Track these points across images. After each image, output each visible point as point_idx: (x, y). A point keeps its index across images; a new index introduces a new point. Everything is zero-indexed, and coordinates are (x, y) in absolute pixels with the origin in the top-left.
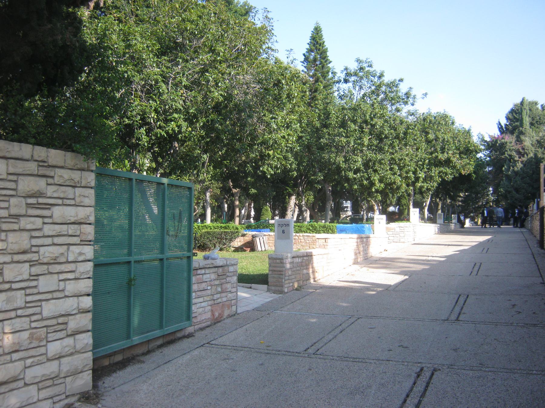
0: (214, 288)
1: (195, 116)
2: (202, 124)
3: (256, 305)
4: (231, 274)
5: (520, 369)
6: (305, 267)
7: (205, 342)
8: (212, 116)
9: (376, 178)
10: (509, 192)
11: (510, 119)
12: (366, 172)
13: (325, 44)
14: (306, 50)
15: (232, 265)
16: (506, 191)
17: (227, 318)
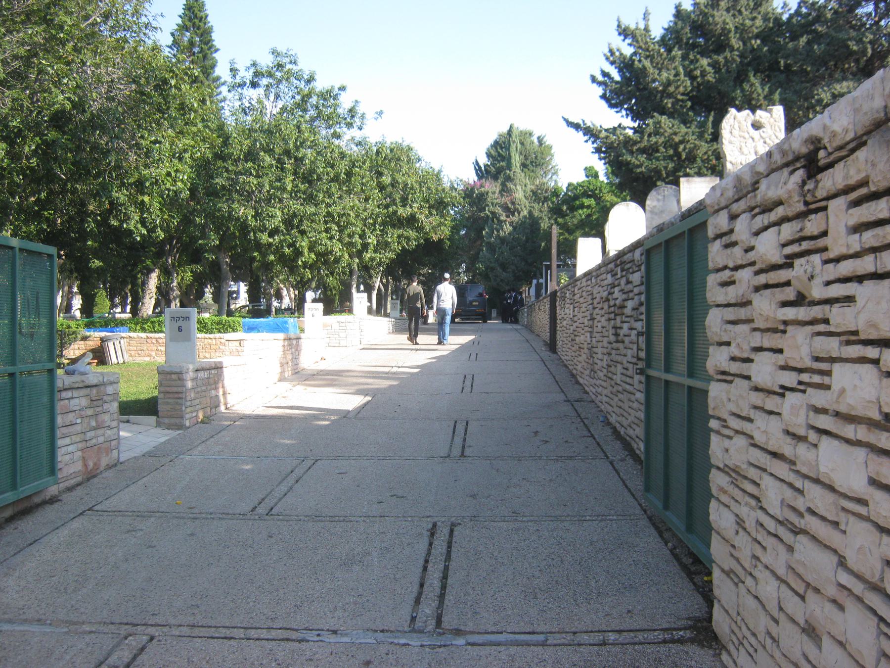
0: (86, 420)
1: (20, 133)
2: (33, 147)
3: (146, 449)
4: (109, 398)
5: (568, 515)
6: (213, 386)
7: (83, 508)
8: (52, 135)
9: (304, 244)
10: (492, 269)
11: (492, 157)
12: (289, 234)
13: (209, 19)
14: (176, 27)
15: (112, 383)
16: (487, 268)
17: (106, 470)
